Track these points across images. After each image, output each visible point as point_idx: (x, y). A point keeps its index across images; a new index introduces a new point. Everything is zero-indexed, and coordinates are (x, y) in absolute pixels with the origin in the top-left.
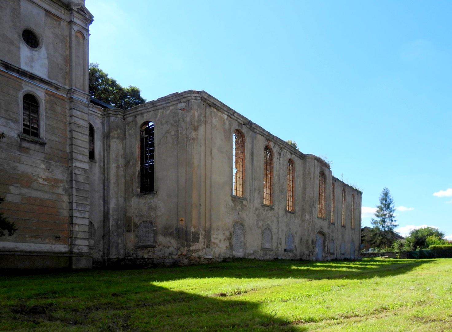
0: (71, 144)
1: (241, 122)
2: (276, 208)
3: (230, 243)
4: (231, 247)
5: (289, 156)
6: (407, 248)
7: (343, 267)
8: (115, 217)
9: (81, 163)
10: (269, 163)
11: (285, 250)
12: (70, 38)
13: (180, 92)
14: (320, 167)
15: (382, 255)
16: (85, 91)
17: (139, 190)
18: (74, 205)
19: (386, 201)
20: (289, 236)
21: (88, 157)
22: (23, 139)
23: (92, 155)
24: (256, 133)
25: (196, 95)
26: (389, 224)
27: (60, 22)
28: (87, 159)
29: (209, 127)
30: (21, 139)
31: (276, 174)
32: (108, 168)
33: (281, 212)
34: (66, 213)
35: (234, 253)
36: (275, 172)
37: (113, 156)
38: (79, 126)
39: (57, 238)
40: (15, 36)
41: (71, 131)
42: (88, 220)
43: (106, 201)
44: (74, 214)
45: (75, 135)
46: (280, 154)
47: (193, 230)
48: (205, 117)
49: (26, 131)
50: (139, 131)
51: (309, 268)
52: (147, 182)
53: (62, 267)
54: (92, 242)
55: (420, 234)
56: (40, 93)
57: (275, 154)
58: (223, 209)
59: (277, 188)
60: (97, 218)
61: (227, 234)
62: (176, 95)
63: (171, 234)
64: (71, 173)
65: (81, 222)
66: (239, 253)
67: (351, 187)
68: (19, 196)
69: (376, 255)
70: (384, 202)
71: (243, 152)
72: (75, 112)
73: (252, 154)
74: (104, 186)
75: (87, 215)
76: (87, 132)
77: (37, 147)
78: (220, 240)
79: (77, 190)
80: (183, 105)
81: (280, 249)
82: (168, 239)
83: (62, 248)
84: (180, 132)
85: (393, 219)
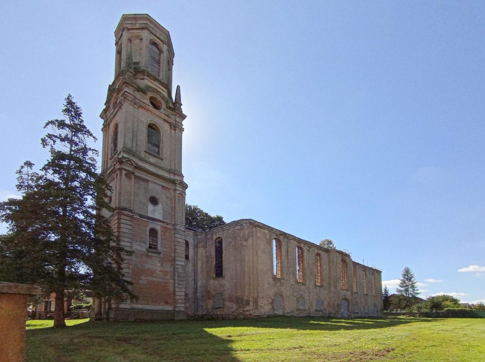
0: (175, 252)
1: (278, 234)
2: (307, 284)
3: (272, 306)
4: (273, 309)
5: (316, 251)
6: (424, 309)
7: (342, 322)
8: (201, 291)
9: (181, 261)
10: (301, 256)
11: (316, 310)
12: (175, 197)
13: (236, 220)
14: (341, 256)
15: (404, 314)
16: (183, 224)
17: (214, 275)
18: (176, 285)
19: (408, 276)
20: (318, 301)
21: (184, 259)
22: (148, 252)
23: (187, 257)
24: (289, 239)
25: (246, 221)
26: (412, 293)
27: (169, 190)
28: (184, 260)
29: (255, 239)
30: (147, 251)
31: (307, 263)
32: (197, 264)
33: (311, 286)
34: (172, 289)
35: (276, 312)
36: (306, 262)
37: (199, 257)
38: (179, 243)
39: (167, 303)
40: (145, 200)
41: (175, 245)
42: (184, 293)
43: (196, 283)
44: (176, 290)
45: (177, 247)
46: (309, 251)
47: (246, 298)
48: (252, 233)
49: (150, 247)
50: (214, 243)
51: (319, 322)
52: (219, 272)
53: (169, 318)
54: (188, 305)
55: (436, 301)
56: (158, 227)
57: (305, 251)
58: (266, 286)
59: (307, 271)
60: (191, 291)
61: (270, 300)
62: (234, 222)
63: (232, 301)
64: (175, 268)
65: (180, 294)
66: (279, 312)
67: (371, 268)
68: (146, 281)
69: (399, 314)
70: (406, 277)
71: (281, 251)
72: (177, 235)
73: (287, 252)
74: (195, 273)
75: (184, 290)
76: (184, 245)
77: (156, 255)
78: (265, 304)
79: (178, 277)
80: (239, 227)
81: (311, 310)
82: (231, 303)
83: (169, 308)
84: (237, 242)
85: (415, 289)
